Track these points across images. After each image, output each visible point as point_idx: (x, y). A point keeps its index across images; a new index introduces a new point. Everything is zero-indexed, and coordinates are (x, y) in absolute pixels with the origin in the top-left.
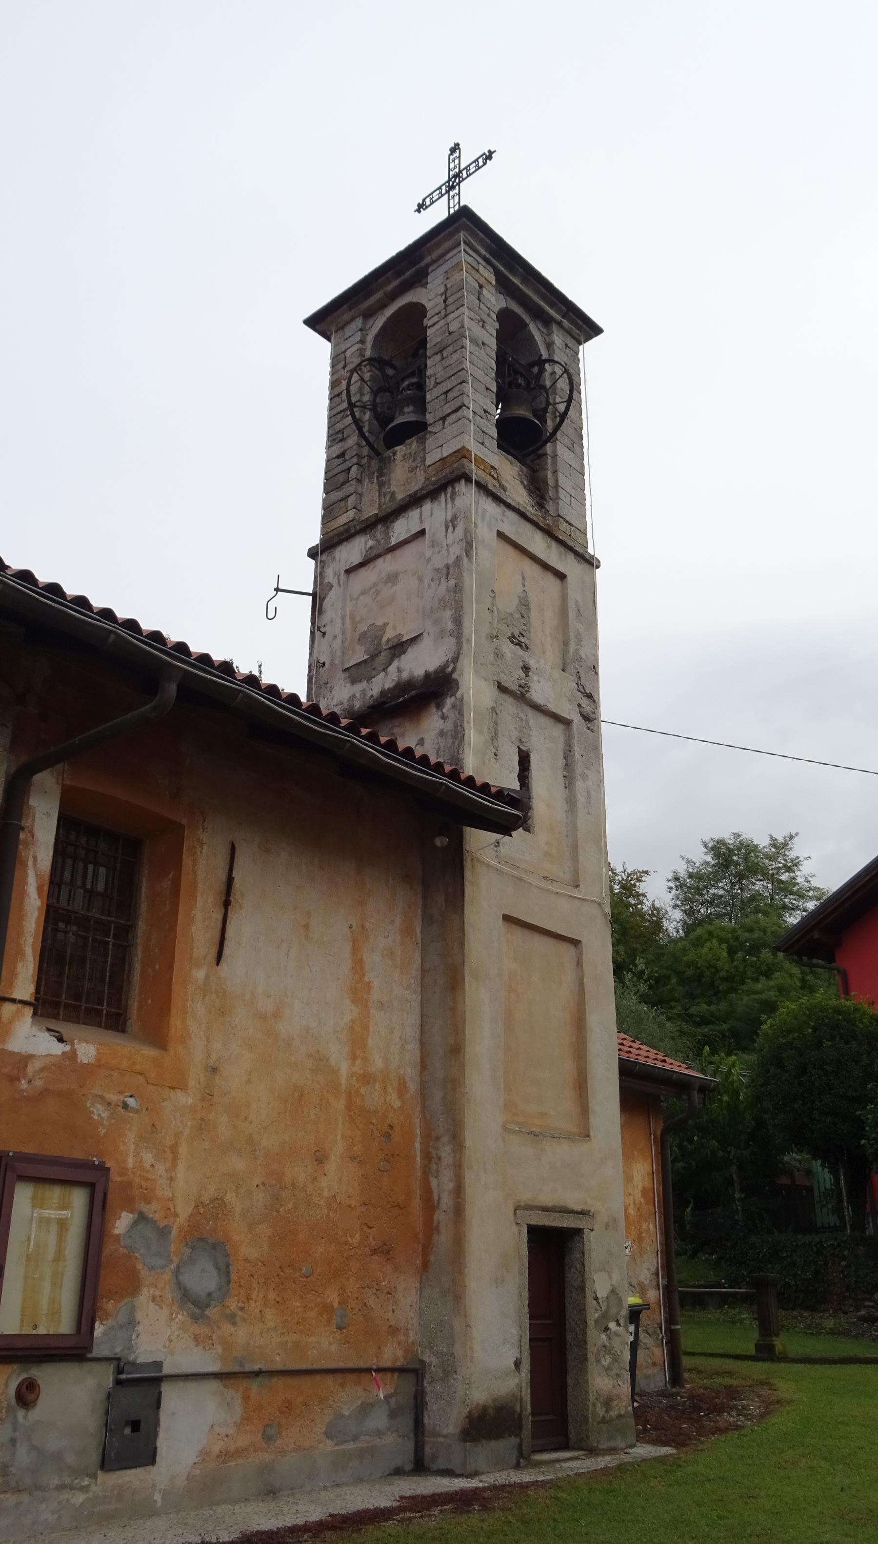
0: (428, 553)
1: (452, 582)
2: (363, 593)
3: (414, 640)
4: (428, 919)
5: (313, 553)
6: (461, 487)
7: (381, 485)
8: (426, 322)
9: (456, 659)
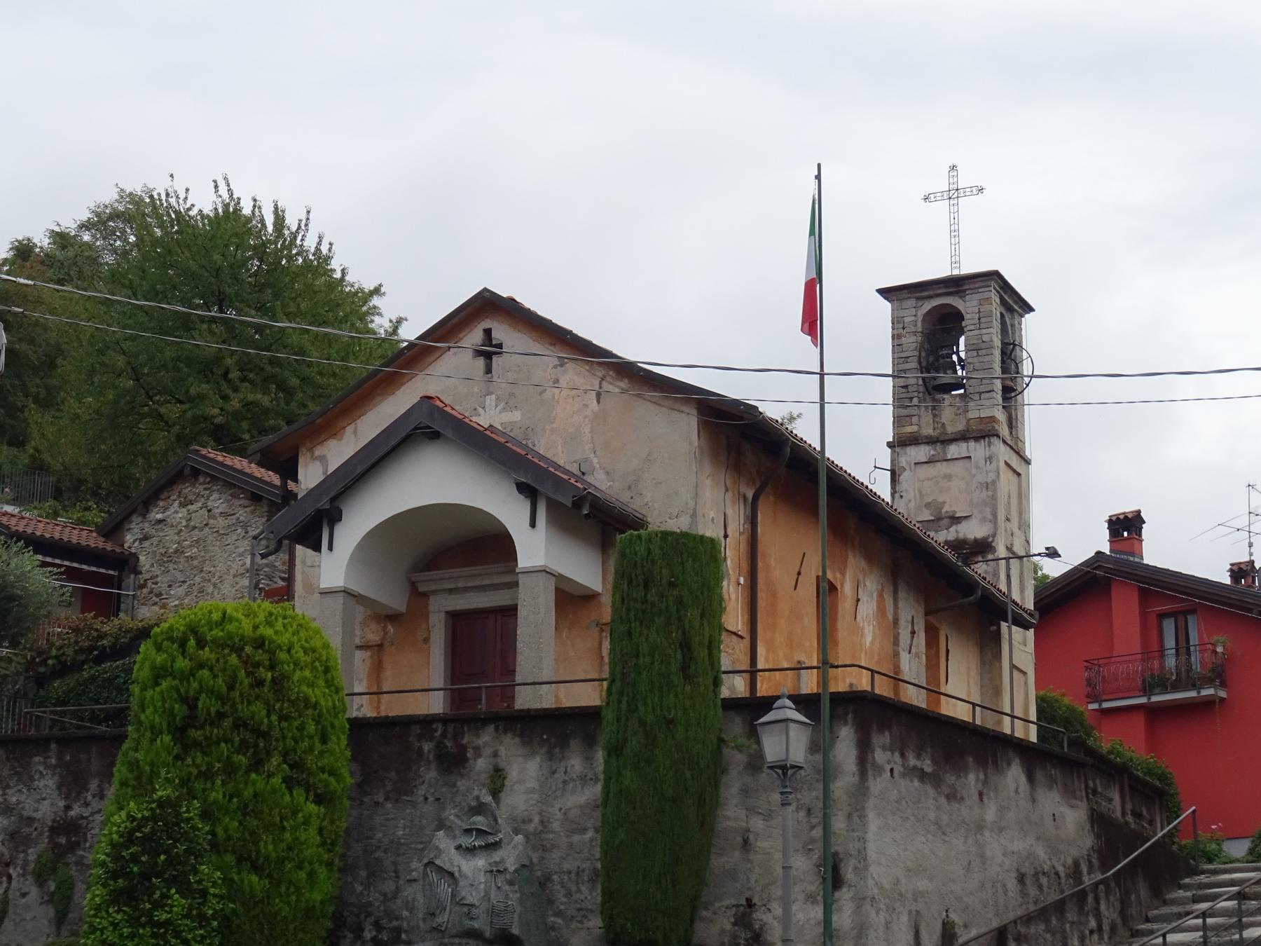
0: (974, 472)
1: (990, 493)
2: (928, 479)
3: (966, 517)
4: (983, 662)
5: (890, 445)
6: (994, 440)
7: (935, 416)
8: (964, 324)
9: (994, 535)
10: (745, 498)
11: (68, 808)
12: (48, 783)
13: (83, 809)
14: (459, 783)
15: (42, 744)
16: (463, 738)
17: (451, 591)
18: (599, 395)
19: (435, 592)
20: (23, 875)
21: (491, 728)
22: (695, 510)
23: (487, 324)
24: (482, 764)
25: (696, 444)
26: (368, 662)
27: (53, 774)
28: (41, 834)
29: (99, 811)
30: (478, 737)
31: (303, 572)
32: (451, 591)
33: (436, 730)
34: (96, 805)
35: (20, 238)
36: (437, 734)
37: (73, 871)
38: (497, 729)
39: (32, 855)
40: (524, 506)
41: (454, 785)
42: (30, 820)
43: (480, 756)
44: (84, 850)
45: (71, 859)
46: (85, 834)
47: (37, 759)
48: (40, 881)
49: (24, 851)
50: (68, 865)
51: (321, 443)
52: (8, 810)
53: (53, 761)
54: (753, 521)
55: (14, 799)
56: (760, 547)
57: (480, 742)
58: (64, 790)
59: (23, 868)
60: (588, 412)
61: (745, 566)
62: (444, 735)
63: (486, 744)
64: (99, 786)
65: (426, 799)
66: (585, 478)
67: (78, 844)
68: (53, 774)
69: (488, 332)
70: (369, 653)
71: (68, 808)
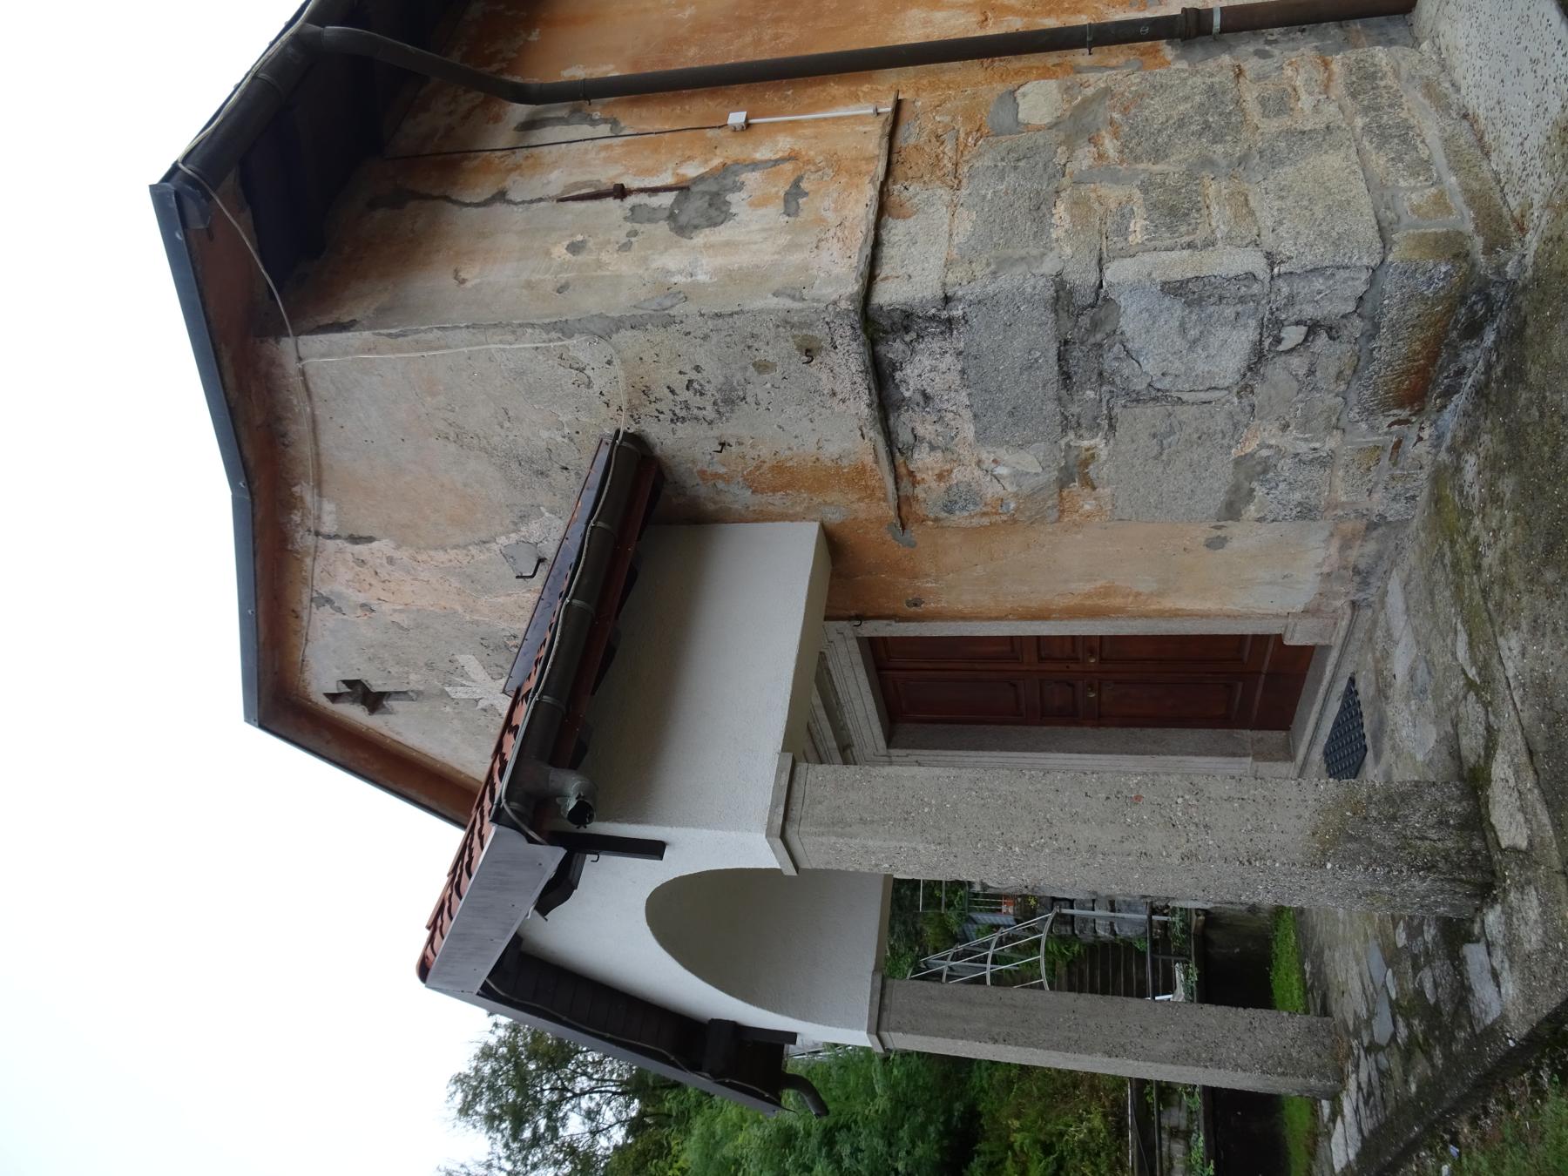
10: (529, 125)
22: (547, 328)
25: (367, 334)
35: (465, 1066)
54: (583, 94)
56: (650, 67)
60: (403, 555)
61: (699, 108)
66: (549, 553)
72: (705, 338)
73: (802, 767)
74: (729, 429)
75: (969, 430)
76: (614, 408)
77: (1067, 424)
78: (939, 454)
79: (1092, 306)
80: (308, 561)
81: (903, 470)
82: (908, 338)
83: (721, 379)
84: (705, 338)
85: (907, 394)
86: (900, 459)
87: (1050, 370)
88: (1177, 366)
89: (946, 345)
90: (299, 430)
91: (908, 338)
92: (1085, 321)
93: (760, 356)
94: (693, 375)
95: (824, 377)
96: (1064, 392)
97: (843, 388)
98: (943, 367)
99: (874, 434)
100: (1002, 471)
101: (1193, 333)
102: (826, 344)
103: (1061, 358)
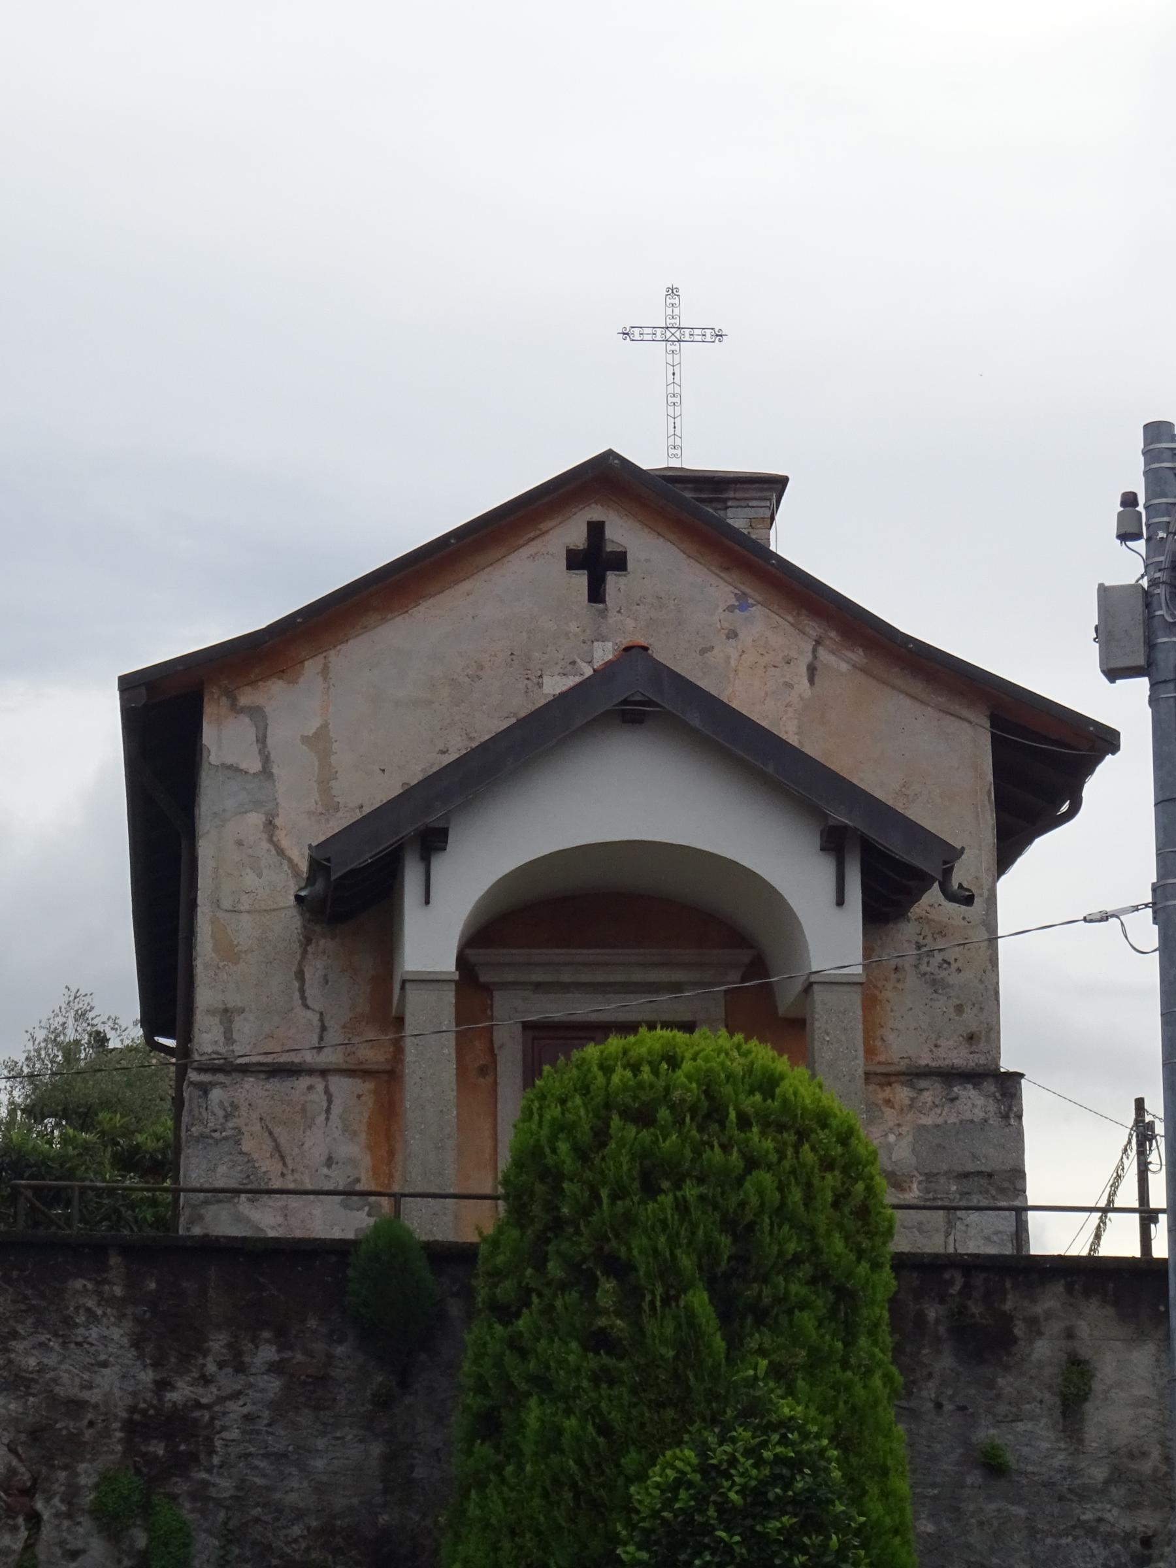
11: (162, 1385)
12: (111, 1334)
13: (200, 1390)
14: (1001, 1381)
15: (90, 1254)
16: (1004, 1300)
17: (538, 986)
18: (812, 670)
19: (504, 986)
20: (69, 1516)
21: (1059, 1287)
23: (595, 513)
24: (1044, 1350)
26: (369, 1100)
27: (121, 1316)
28: (106, 1433)
29: (236, 1396)
30: (1034, 1301)
31: (214, 921)
32: (538, 986)
33: (951, 1283)
34: (228, 1381)
36: (954, 1290)
37: (187, 1511)
38: (1070, 1290)
39: (87, 1474)
40: (822, 871)
41: (991, 1385)
42: (75, 1407)
43: (1040, 1334)
44: (209, 1471)
45: (181, 1486)
46: (209, 1440)
47: (78, 1284)
48: (111, 1523)
49: (65, 1467)
50: (174, 1498)
51: (252, 683)
52: (19, 1383)
53: (118, 1291)
55: (32, 1362)
57: (1039, 1309)
58: (149, 1349)
59: (68, 1499)
62: (967, 1288)
63: (1049, 1315)
64: (229, 1346)
65: (939, 1406)
67: (194, 1458)
68: (121, 1316)
69: (596, 530)
70: (369, 1085)
71: (162, 1385)
72: (981, 981)
73: (859, 989)
74: (911, 980)
75: (926, 1121)
76: (928, 909)
77: (930, 1177)
78: (907, 1102)
79: (1015, 1188)
80: (790, 618)
81: (893, 1079)
82: (997, 1094)
83: (951, 983)
84: (981, 981)
85: (955, 1089)
86: (903, 1078)
87: (970, 1167)
88: (972, 1232)
89: (991, 1114)
90: (917, 687)
91: (997, 1094)
92: (1006, 1185)
93: (967, 1010)
94: (954, 966)
95: (951, 1043)
96: (955, 1174)
97: (941, 1052)
98: (976, 1111)
99: (902, 1066)
100: (892, 1138)
101: (995, 1238)
102: (974, 1048)
103: (979, 1173)
